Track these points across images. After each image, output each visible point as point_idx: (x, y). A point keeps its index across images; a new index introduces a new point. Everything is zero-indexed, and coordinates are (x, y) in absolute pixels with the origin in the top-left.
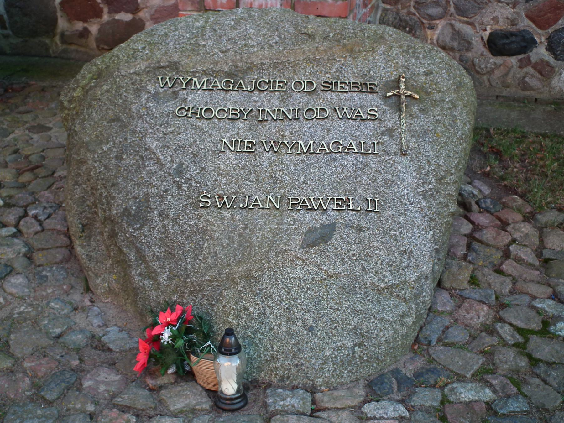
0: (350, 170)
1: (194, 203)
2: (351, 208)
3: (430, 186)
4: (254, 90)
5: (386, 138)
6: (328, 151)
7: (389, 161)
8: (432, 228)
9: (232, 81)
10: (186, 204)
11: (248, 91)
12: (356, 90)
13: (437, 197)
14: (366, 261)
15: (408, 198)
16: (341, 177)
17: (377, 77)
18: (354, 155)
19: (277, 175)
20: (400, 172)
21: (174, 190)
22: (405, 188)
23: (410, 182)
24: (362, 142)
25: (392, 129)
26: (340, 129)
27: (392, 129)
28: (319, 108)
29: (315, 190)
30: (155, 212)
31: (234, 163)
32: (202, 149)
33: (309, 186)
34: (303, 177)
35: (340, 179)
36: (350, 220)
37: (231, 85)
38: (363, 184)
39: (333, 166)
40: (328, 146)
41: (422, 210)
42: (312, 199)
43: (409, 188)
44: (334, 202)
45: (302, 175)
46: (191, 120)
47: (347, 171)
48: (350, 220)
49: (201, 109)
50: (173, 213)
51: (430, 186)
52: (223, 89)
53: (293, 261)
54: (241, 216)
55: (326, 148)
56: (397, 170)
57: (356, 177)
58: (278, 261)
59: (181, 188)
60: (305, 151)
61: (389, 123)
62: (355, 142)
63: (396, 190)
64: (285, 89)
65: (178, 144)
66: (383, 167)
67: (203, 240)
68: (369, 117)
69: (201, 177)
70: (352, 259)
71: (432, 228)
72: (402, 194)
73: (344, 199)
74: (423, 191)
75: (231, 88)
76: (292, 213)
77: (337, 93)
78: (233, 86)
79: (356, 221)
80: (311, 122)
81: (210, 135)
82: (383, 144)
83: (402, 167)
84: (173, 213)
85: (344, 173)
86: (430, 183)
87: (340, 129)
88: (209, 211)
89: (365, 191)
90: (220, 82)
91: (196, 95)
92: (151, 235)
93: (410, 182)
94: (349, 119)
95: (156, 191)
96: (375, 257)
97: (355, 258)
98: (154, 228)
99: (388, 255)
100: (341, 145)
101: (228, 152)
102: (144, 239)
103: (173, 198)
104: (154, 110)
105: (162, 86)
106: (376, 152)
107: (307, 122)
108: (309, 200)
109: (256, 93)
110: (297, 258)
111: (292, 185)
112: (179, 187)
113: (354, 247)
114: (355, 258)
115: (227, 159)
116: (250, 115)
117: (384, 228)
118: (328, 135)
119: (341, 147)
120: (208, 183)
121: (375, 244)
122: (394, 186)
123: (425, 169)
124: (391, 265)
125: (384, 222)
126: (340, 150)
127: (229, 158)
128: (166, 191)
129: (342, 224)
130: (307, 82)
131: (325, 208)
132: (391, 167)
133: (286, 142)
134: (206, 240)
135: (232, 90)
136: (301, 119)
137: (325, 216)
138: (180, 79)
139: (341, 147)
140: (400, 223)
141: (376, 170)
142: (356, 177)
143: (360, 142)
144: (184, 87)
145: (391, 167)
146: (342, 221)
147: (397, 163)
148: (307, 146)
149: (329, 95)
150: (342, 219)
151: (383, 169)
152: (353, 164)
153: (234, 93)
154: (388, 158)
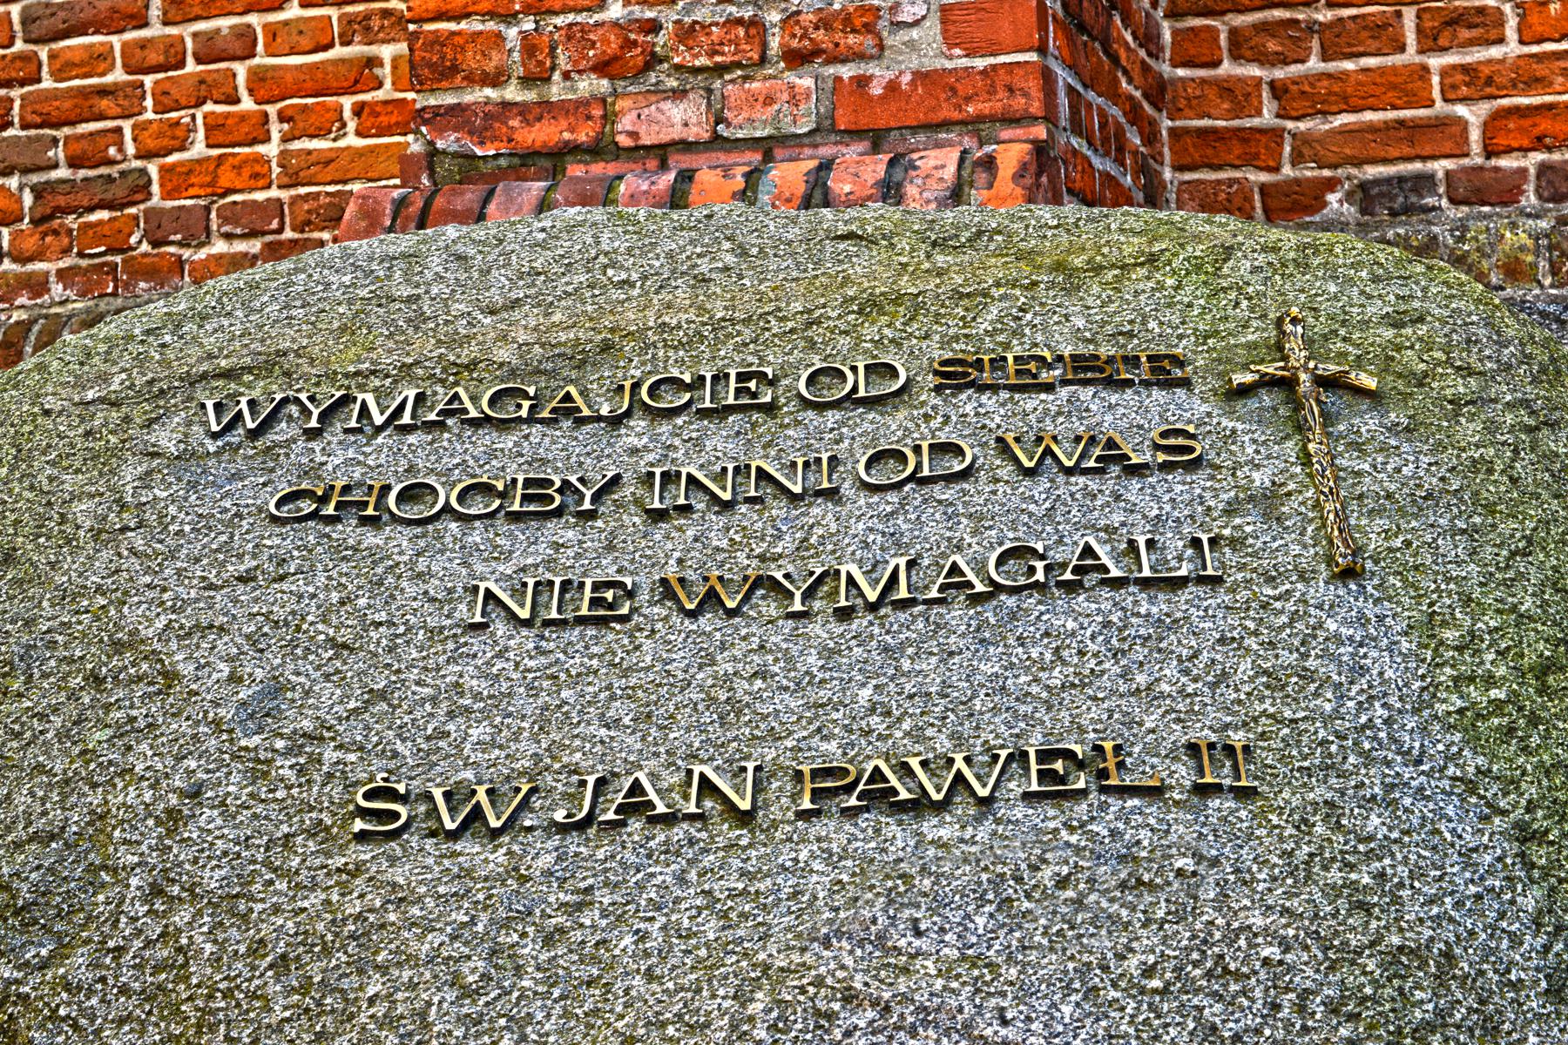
0: (1092, 647)
1: (327, 829)
2: (1113, 782)
3: (1494, 693)
4: (628, 414)
5: (1249, 523)
6: (980, 588)
7: (1278, 605)
8: (1536, 873)
9: (531, 391)
10: (287, 836)
11: (599, 419)
12: (1098, 375)
13: (1535, 740)
14: (1218, 997)
15: (1391, 738)
16: (1056, 677)
17: (1180, 337)
18: (1105, 593)
19: (740, 693)
20: (1338, 639)
21: (235, 786)
22: (1371, 698)
23: (1389, 673)
24: (1141, 541)
25: (1274, 495)
26: (1032, 507)
27: (1274, 495)
28: (925, 445)
29: (930, 732)
30: (134, 881)
31: (531, 664)
32: (381, 624)
33: (899, 720)
34: (866, 693)
35: (1048, 688)
36: (1114, 833)
37: (526, 404)
38: (1162, 695)
39: (1011, 641)
40: (980, 569)
41: (1473, 792)
42: (914, 763)
43: (1393, 700)
44: (1027, 769)
45: (864, 685)
46: (337, 531)
47: (1081, 653)
48: (1114, 833)
49: (386, 489)
50: (218, 874)
51: (1494, 693)
52: (488, 419)
53: (830, 1016)
54: (559, 859)
55: (971, 576)
56: (1321, 634)
57: (1125, 675)
58: (751, 1019)
59: (266, 774)
60: (872, 596)
61: (1256, 475)
62: (1108, 548)
63: (1328, 707)
64: (768, 399)
65: (267, 616)
66: (1251, 625)
67: (361, 972)
68: (1161, 457)
69: (367, 728)
70: (1143, 991)
71: (1536, 873)
72: (1363, 719)
73: (1077, 749)
74: (1461, 711)
75: (524, 413)
76: (818, 828)
77: (1004, 395)
78: (532, 407)
79: (1144, 835)
80: (893, 497)
81: (420, 575)
82: (1236, 543)
83: (1345, 622)
84: (218, 874)
85: (1064, 663)
86: (1490, 681)
87: (1032, 507)
88: (399, 852)
89: (1178, 720)
90: (475, 399)
91: (368, 450)
92: (103, 980)
93: (1389, 673)
94: (1069, 472)
95: (148, 796)
96: (1263, 975)
97: (1156, 983)
98: (119, 951)
99: (1332, 968)
100: (1042, 557)
101: (500, 628)
102: (69, 1004)
103: (228, 816)
104: (172, 510)
105: (215, 428)
106: (1210, 572)
107: (876, 499)
108: (905, 770)
109: (639, 423)
110: (850, 998)
111: (812, 728)
112: (259, 769)
113: (1149, 938)
114: (1156, 983)
115: (500, 655)
116: (608, 500)
117: (1291, 854)
118: (974, 533)
119: (1040, 565)
120: (399, 747)
121: (1258, 921)
122: (1316, 695)
123: (1458, 627)
124: (1354, 1017)
125: (1290, 831)
126: (1040, 576)
127: (507, 649)
128: (195, 793)
129: (1078, 850)
130: (867, 367)
131: (983, 792)
132: (1290, 624)
133: (779, 576)
134: (377, 967)
135: (531, 420)
136: (847, 489)
137: (989, 825)
138: (297, 401)
139: (1040, 565)
140: (1370, 838)
141: (1222, 641)
142: (1125, 675)
143: (1131, 542)
144: (314, 423)
145: (1290, 624)
146: (1074, 839)
147: (1320, 607)
148: (877, 581)
149: (967, 403)
150: (1072, 830)
151: (1256, 633)
152: (1107, 624)
153: (536, 429)
154: (1270, 592)
